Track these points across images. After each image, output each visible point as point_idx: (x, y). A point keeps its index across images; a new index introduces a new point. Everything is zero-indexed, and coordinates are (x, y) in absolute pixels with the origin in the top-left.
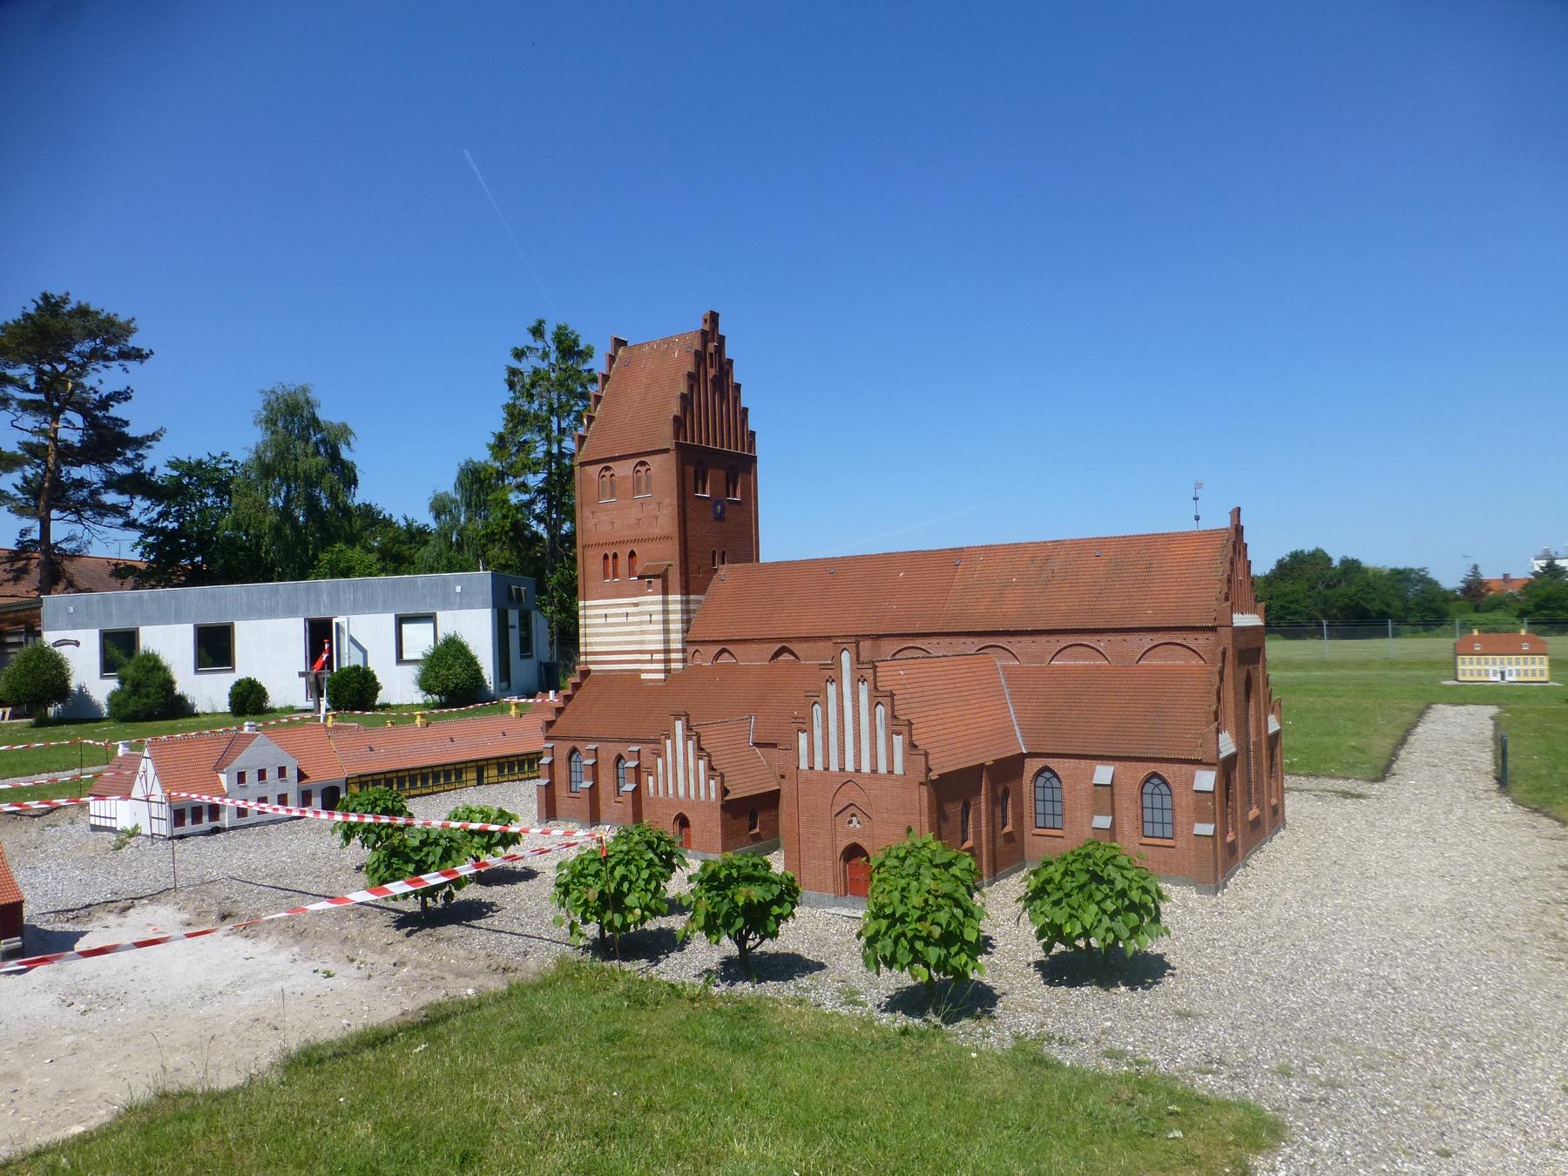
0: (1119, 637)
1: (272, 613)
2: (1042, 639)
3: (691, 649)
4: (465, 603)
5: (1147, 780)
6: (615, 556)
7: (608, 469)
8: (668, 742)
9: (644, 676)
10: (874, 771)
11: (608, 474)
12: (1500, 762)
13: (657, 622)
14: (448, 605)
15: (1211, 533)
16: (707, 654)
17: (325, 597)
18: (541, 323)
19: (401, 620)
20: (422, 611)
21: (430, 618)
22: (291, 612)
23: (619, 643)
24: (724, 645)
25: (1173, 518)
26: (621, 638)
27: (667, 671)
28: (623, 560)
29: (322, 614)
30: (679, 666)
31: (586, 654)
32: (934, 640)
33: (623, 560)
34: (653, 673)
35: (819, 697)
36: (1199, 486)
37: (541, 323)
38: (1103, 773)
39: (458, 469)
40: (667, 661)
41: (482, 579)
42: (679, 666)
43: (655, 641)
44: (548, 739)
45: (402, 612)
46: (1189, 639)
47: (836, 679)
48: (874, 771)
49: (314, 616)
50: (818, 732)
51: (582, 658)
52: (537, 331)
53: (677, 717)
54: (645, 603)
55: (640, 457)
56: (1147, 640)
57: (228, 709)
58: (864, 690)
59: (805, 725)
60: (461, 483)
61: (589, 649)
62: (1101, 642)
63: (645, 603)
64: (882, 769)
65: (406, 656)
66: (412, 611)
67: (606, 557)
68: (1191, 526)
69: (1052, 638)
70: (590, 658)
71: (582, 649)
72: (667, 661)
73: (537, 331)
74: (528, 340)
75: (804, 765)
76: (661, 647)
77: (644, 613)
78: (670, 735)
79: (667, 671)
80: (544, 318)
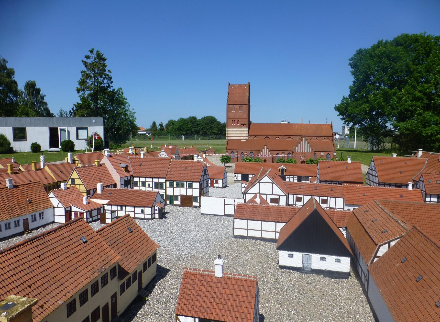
0: (320, 137)
1: (38, 125)
2: (309, 137)
3: (249, 136)
4: (96, 124)
5: (327, 154)
6: (235, 121)
7: (241, 106)
8: (263, 149)
9: (241, 140)
10: (307, 152)
11: (234, 107)
12: (12, 247)
13: (245, 132)
14: (91, 125)
15: (328, 124)
16: (252, 138)
17: (55, 121)
18: (93, 49)
19: (78, 129)
20: (84, 126)
21: (86, 128)
22: (44, 125)
23: (235, 135)
24: (256, 136)
25: (323, 122)
26: (234, 134)
27: (246, 140)
28: (236, 121)
29: (55, 126)
30: (248, 139)
31: (227, 136)
32: (293, 137)
33: (236, 121)
34: (243, 140)
35: (300, 143)
36: (327, 118)
37: (93, 49)
38: (322, 153)
39: (25, 82)
40: (246, 138)
41: (101, 119)
42: (248, 139)
43: (244, 135)
44: (227, 150)
45: (78, 126)
46: (329, 138)
47: (302, 141)
48: (307, 152)
49: (51, 126)
50: (299, 147)
51: (227, 137)
52: (92, 52)
53: (265, 146)
54: (242, 129)
55: (241, 105)
56: (324, 138)
57: (31, 151)
58: (306, 142)
59: (297, 146)
60: (26, 87)
61: (228, 136)
62: (317, 138)
63: (242, 129)
64: (308, 151)
65: (79, 138)
66: (81, 126)
67: (233, 121)
68: (325, 123)
69: (311, 137)
70: (228, 137)
71: (227, 136)
72: (246, 138)
73: (92, 52)
74: (89, 54)
75: (297, 151)
76: (245, 136)
77: (242, 130)
78: (264, 148)
79: (246, 140)
80: (94, 48)
